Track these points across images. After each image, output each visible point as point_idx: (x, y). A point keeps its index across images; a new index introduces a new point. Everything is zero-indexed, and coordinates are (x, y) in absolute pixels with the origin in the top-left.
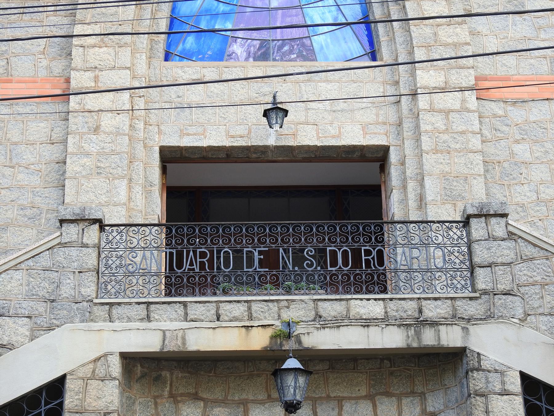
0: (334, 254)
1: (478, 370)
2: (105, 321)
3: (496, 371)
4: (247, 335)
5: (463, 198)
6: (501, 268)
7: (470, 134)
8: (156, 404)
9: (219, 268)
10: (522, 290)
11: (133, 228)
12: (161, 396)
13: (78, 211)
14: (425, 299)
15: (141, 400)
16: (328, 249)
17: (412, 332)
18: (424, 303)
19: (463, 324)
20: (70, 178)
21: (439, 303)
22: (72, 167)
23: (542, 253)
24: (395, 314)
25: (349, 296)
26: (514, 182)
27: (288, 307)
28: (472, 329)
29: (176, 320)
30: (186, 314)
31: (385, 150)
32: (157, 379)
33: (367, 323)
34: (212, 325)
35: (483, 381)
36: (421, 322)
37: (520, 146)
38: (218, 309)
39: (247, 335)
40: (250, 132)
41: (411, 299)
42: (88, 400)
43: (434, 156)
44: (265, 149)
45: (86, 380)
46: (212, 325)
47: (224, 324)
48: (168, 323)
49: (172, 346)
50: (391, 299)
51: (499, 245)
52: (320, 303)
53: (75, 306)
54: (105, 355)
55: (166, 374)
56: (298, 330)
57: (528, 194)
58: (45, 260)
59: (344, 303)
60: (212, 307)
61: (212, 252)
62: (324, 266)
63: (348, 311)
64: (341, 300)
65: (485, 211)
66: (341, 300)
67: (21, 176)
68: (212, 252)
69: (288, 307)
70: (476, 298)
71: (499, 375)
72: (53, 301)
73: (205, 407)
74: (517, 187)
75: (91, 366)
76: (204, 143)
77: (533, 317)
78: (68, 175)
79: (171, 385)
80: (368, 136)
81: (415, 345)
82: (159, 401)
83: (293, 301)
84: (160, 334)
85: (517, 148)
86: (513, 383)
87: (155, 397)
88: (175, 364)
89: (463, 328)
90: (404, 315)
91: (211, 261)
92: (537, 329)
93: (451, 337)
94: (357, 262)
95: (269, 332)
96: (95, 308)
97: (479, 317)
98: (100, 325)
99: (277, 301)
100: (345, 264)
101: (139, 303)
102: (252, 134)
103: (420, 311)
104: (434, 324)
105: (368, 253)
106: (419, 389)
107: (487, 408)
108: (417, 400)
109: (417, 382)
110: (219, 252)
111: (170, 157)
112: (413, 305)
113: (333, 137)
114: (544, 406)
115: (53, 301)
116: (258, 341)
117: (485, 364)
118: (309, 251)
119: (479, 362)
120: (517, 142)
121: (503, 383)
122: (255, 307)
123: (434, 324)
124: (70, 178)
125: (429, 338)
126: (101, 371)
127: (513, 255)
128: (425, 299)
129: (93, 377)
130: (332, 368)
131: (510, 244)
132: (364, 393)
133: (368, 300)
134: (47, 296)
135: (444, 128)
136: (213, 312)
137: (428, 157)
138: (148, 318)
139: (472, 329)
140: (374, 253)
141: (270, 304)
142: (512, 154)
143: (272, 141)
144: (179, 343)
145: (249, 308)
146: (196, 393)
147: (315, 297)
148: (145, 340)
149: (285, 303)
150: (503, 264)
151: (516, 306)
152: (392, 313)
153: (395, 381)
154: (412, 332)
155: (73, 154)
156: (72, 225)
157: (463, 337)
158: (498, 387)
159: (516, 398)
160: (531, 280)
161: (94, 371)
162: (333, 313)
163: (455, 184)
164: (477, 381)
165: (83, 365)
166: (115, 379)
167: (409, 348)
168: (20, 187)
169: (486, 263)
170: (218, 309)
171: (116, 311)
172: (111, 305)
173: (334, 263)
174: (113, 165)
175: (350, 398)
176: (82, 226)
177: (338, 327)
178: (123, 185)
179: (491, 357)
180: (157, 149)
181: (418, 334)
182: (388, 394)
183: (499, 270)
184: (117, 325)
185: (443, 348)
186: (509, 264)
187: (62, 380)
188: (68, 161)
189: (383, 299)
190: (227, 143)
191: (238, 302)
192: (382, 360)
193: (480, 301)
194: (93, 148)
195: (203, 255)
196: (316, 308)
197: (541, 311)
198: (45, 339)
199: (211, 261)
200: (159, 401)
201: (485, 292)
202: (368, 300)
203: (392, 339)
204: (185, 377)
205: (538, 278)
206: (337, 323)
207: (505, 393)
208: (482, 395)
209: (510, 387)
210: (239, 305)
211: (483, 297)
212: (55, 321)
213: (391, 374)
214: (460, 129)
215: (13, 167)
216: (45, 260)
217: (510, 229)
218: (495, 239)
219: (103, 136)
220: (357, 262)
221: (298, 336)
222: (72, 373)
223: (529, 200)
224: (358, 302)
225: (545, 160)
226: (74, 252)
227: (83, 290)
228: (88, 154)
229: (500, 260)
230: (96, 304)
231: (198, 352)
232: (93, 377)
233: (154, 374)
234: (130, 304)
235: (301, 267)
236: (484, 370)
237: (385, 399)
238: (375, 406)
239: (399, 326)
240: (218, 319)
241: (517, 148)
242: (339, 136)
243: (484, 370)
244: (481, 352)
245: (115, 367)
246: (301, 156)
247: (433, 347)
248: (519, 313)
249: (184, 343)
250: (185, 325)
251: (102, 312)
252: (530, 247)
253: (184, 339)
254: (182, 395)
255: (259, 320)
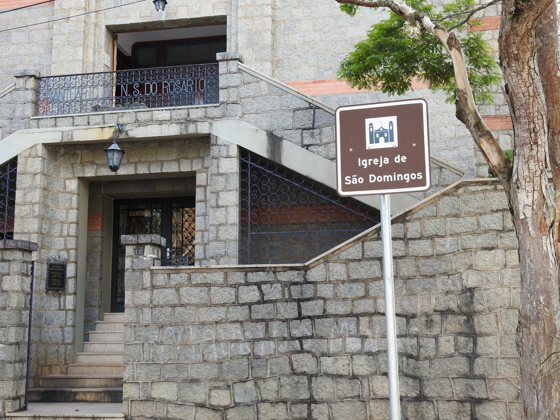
0: (148, 86)
1: (215, 145)
2: (35, 128)
3: (225, 145)
4: (102, 131)
5: (258, 44)
6: (232, 89)
7: (265, 6)
8: (73, 167)
9: (198, 89)
10: (242, 100)
11: (74, 77)
12: (76, 163)
13: (23, 72)
14: (191, 108)
15: (64, 166)
16: (146, 83)
17: (183, 126)
18: (191, 110)
19: (210, 121)
20: (55, 48)
21: (198, 110)
22: (56, 42)
23: (255, 79)
24: (175, 117)
25: (153, 109)
26: (291, 32)
27: (122, 116)
28: (214, 123)
29: (68, 126)
30: (73, 122)
31: (225, 17)
32: (74, 154)
33: (161, 122)
34: (85, 127)
35: (217, 151)
36: (188, 121)
37: (297, 10)
38: (89, 119)
39: (102, 131)
40: (152, 14)
41: (184, 109)
42: (27, 168)
43: (244, 21)
44: (161, 22)
45: (26, 158)
46: (85, 127)
47: (91, 127)
48: (65, 128)
49: (66, 140)
50: (174, 109)
51: (233, 76)
52: (138, 113)
53: (22, 121)
54: (35, 145)
55: (79, 152)
56: (127, 128)
57: (299, 39)
58: (8, 98)
59: (150, 112)
60: (86, 118)
61: (194, 81)
62: (143, 93)
63: (152, 117)
64: (149, 111)
65: (226, 58)
66: (149, 111)
67: (34, 48)
68: (194, 81)
69: (122, 116)
70: (218, 106)
71: (226, 147)
72: (12, 119)
73: (97, 168)
74: (293, 35)
75: (29, 151)
76: (128, 22)
77: (247, 115)
78: (54, 46)
79: (81, 157)
80: (215, 11)
81: (184, 133)
82: (74, 166)
83: (125, 113)
84: (61, 133)
85: (295, 12)
86: (233, 151)
87: (72, 164)
88: (83, 146)
89: (210, 123)
90: (180, 118)
91: (194, 86)
92: (249, 122)
93: (203, 128)
94: (160, 91)
95: (113, 130)
96: (31, 121)
97: (218, 116)
98: (33, 130)
99: (117, 113)
100: (154, 91)
101: (51, 118)
102: (153, 15)
103: (188, 115)
104: (195, 122)
105: (166, 84)
106: (202, 155)
107: (218, 165)
108: (200, 161)
109: (201, 151)
110: (198, 81)
111: (114, 32)
112: (185, 112)
113: (196, 13)
114: (249, 163)
115: (12, 119)
116: (107, 134)
117: (219, 142)
118: (136, 85)
119: (216, 141)
120: (295, 7)
121: (228, 151)
122: (106, 117)
123: (195, 122)
124: (55, 48)
125: (192, 129)
126: (33, 153)
127: (239, 82)
128: (191, 108)
129: (30, 156)
130: (160, 145)
131: (238, 75)
132: (175, 158)
133: (162, 110)
134: (9, 116)
135: (251, 3)
136: (86, 120)
137: (241, 21)
138: (56, 125)
139: (214, 123)
140: (169, 84)
141: (114, 115)
142: (292, 15)
143: (163, 18)
144: (70, 137)
145: (104, 118)
146: (93, 161)
147: (136, 110)
148: (54, 137)
149: (121, 114)
150: (234, 87)
151: (238, 110)
152: (174, 117)
153: (190, 151)
154: (183, 126)
155: (56, 34)
156: (21, 79)
157: (209, 128)
158: (225, 154)
159: (234, 159)
160: (248, 95)
161: (30, 154)
162: (144, 118)
163: (254, 36)
164: (214, 151)
165: (25, 151)
166: (39, 157)
167: (181, 135)
168: (34, 54)
169: (225, 87)
170: (89, 119)
171: (41, 122)
172: (38, 119)
173: (148, 91)
174: (76, 39)
175: (167, 161)
176: (25, 79)
177: (147, 125)
178: (80, 50)
179: (222, 138)
180: (104, 27)
181: (186, 127)
182: (186, 158)
183: (231, 90)
184: (41, 129)
185: (198, 134)
186: (236, 87)
187: (16, 158)
188: (54, 38)
189: (170, 110)
190: (140, 21)
191: (98, 115)
192: (185, 140)
193: (220, 108)
194: (66, 31)
195: (190, 82)
196: (136, 116)
197: (251, 111)
198: (9, 138)
199: (194, 86)
200: (74, 166)
201: (223, 103)
202: (162, 110)
203: (173, 130)
204: (87, 153)
205: (252, 94)
206: (146, 123)
207: (228, 157)
208: (216, 158)
209: (231, 154)
210: (98, 116)
211: (222, 105)
212: (13, 129)
213: (189, 147)
214: (260, 3)
215: (30, 43)
216: (8, 98)
217: (239, 67)
218: (230, 73)
219: (71, 23)
220: (160, 91)
221: (126, 131)
222: (20, 154)
223: (299, 42)
224: (157, 111)
225: (310, 17)
226: (21, 93)
227: (25, 113)
228: (63, 34)
229: (232, 85)
230: (31, 119)
231: (79, 141)
232: (30, 156)
233: (72, 152)
234: (47, 118)
235: (132, 94)
236: (218, 145)
237: (185, 161)
238: (179, 164)
239: (177, 123)
240: (88, 125)
241: (295, 12)
242: (199, 12)
243: (218, 145)
244: (218, 136)
245: (40, 150)
246: (184, 24)
247: (193, 134)
248: (240, 113)
249: (72, 138)
250: (73, 128)
251: (34, 123)
252: (249, 76)
253: (72, 135)
254: (87, 162)
255: (108, 123)
